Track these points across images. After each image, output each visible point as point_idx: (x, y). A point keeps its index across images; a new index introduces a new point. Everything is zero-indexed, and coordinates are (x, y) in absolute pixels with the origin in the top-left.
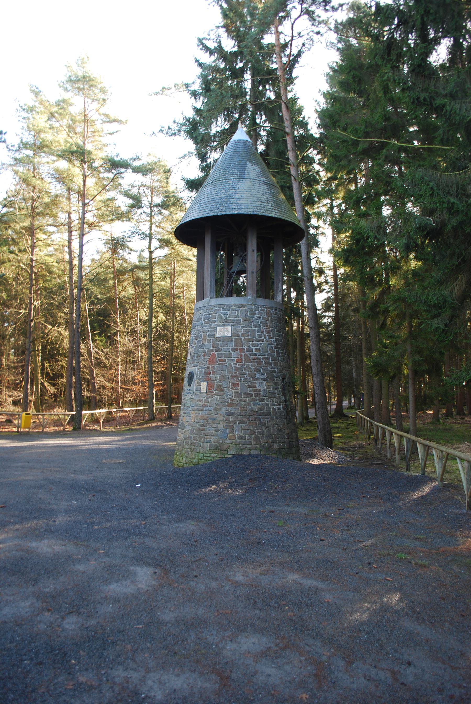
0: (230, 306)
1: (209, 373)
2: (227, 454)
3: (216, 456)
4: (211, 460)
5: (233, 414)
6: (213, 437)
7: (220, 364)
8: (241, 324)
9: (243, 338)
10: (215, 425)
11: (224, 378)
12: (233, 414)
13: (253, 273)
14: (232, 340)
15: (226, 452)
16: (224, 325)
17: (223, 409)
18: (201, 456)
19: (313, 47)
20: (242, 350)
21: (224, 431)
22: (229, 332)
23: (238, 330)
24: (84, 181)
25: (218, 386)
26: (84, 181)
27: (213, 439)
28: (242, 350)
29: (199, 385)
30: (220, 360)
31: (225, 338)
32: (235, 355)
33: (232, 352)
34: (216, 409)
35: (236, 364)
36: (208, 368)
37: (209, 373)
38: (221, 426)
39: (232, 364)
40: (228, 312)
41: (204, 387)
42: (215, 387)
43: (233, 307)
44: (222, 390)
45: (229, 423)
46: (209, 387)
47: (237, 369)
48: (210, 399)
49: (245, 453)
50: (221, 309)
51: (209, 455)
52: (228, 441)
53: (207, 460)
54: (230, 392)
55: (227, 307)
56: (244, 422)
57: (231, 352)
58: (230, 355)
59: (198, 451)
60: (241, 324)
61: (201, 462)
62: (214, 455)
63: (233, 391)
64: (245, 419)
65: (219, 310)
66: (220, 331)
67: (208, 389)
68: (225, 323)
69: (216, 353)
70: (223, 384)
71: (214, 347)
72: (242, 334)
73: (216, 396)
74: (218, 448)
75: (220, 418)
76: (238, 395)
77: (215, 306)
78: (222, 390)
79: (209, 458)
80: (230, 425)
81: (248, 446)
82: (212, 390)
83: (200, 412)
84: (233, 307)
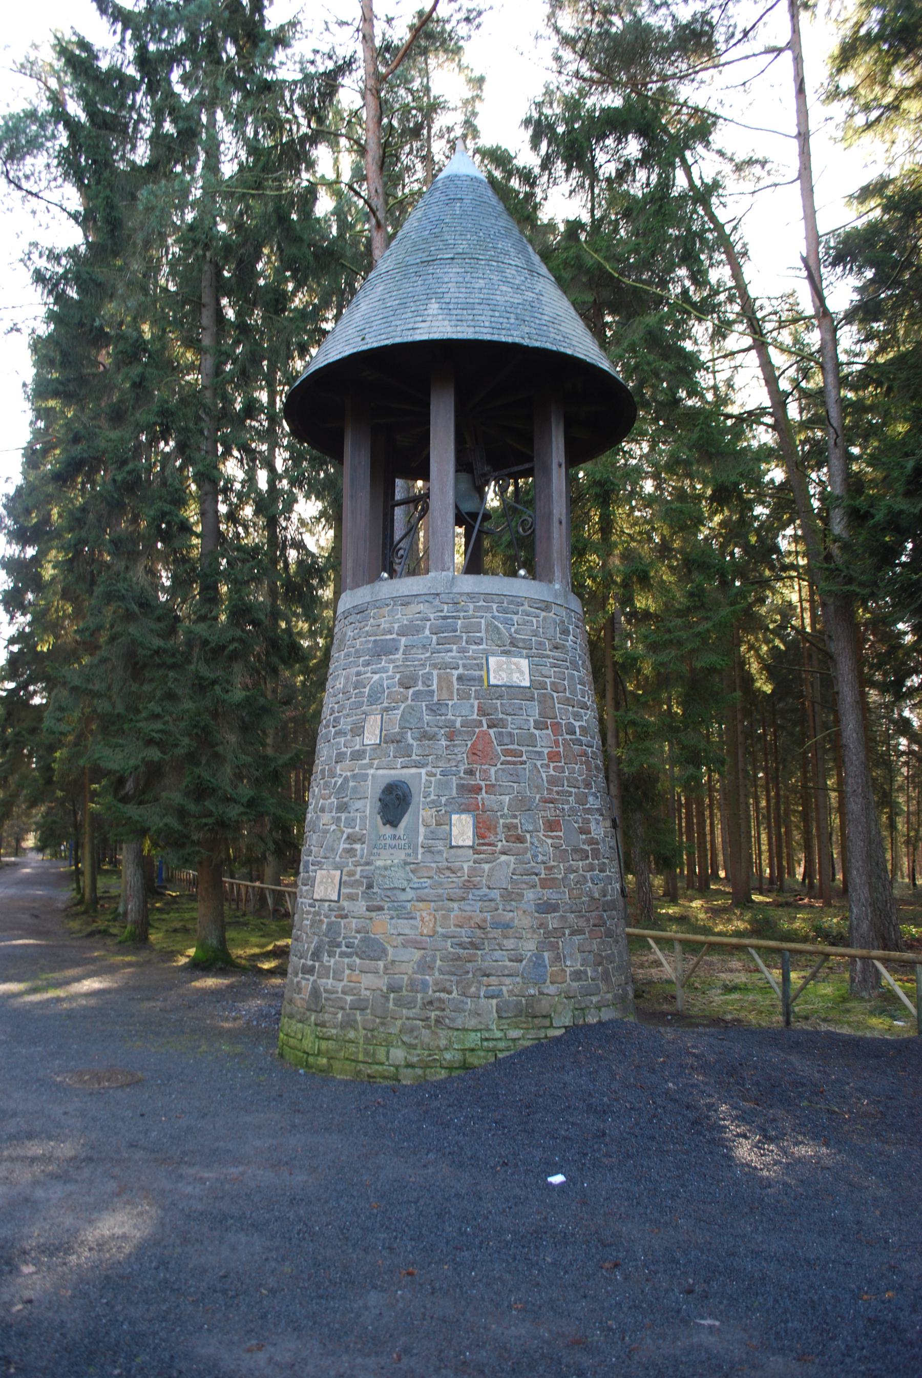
0: (516, 601)
1: (478, 790)
2: (551, 1026)
3: (523, 1037)
4: (508, 1049)
5: (554, 908)
6: (507, 981)
7: (508, 763)
8: (548, 657)
9: (555, 695)
10: (509, 943)
11: (522, 804)
12: (554, 908)
13: (561, 523)
14: (532, 699)
15: (547, 1022)
16: (506, 653)
17: (530, 895)
18: (473, 1039)
19: (28, 78)
20: (556, 727)
21: (538, 962)
22: (522, 673)
23: (545, 671)
24: (796, 31)
25: (509, 827)
26: (796, 31)
27: (508, 986)
28: (556, 727)
29: (443, 821)
30: (507, 753)
31: (512, 689)
32: (544, 740)
33: (537, 732)
34: (509, 896)
35: (548, 766)
36: (470, 772)
37: (478, 790)
38: (529, 946)
39: (539, 763)
40: (515, 617)
41: (462, 829)
42: (500, 829)
43: (526, 607)
44: (520, 839)
45: (548, 934)
46: (483, 830)
47: (552, 781)
48: (486, 867)
49: (592, 1020)
50: (495, 606)
51: (499, 1034)
52: (551, 989)
53: (493, 1050)
54: (544, 845)
55: (511, 603)
56: (580, 932)
57: (533, 730)
58: (531, 741)
59: (459, 1024)
60: (548, 657)
61: (473, 1060)
62: (514, 1033)
63: (549, 841)
64: (582, 923)
65: (488, 609)
66: (499, 668)
67: (479, 834)
68: (512, 647)
69: (491, 731)
70: (523, 822)
71: (482, 712)
72: (553, 683)
73: (504, 858)
74: (528, 1012)
75: (522, 919)
76: (562, 855)
77: (471, 596)
78: (520, 839)
79: (501, 1045)
80: (550, 940)
81: (595, 999)
82: (492, 838)
83: (455, 905)
84: (526, 607)
